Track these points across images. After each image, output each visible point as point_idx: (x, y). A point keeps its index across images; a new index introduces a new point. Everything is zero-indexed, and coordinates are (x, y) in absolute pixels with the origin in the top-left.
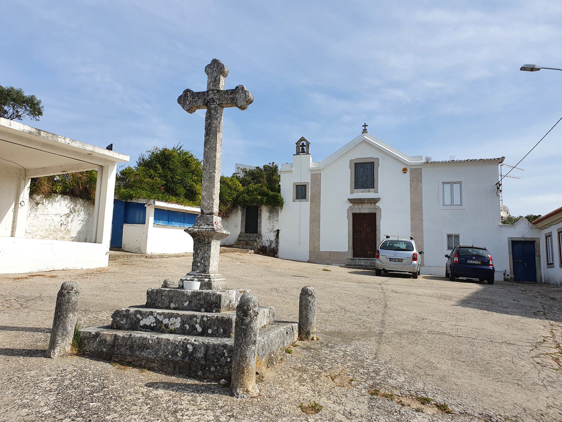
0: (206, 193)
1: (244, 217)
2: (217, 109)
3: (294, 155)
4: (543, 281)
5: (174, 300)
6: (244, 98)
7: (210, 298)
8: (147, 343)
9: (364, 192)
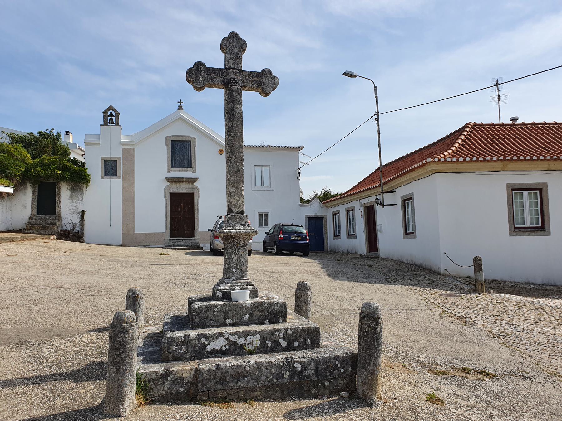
0: (233, 188)
1: (36, 196)
3: (101, 125)
4: (329, 250)
5: (230, 314)
7: (274, 307)
8: (243, 371)
9: (182, 171)
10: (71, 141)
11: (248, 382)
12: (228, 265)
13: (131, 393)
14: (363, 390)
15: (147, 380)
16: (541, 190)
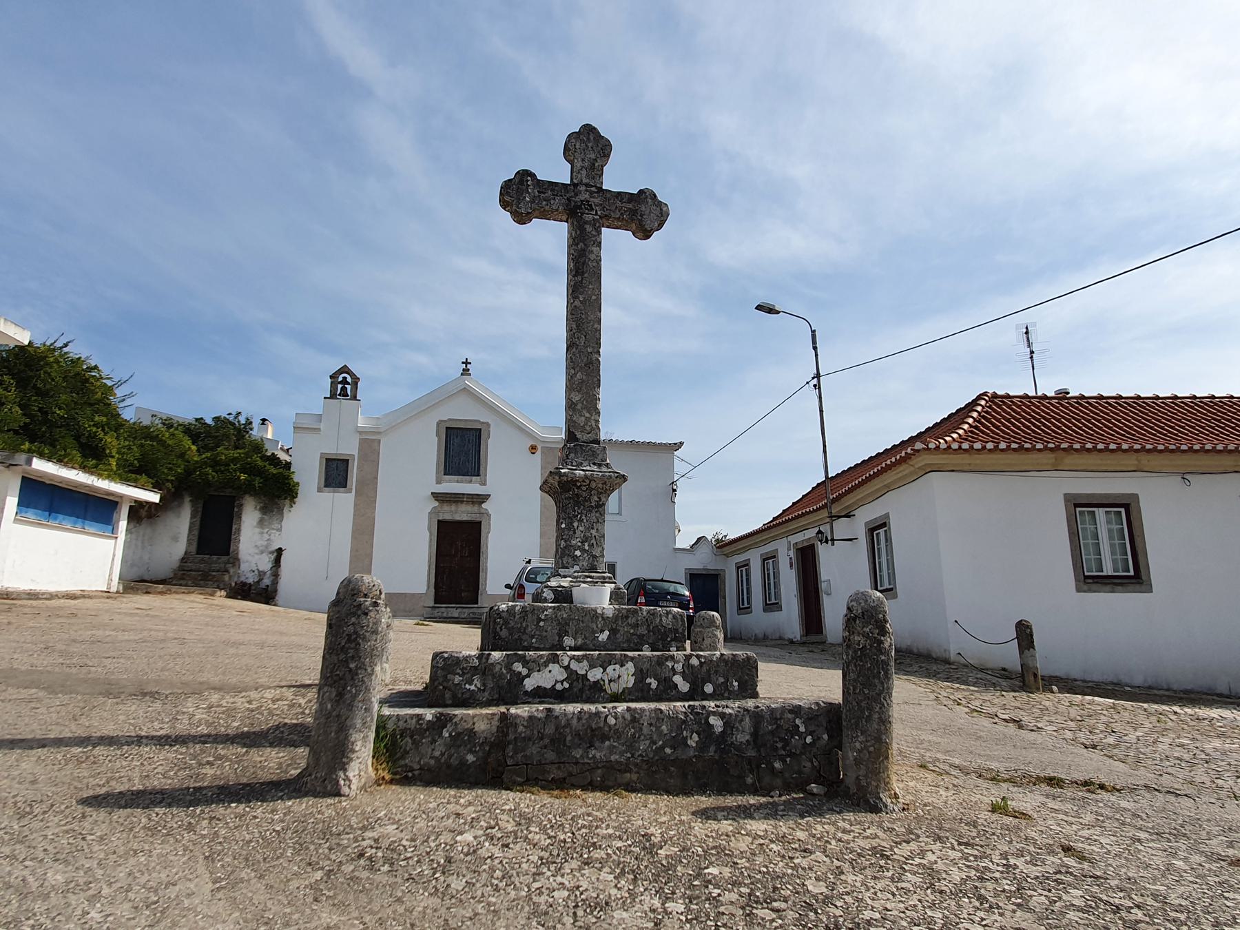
2: (597, 224)
3: (325, 398)
5: (572, 628)
6: (658, 216)
7: (661, 620)
8: (602, 724)
9: (462, 482)
10: (269, 436)
11: (612, 749)
12: (565, 542)
13: (363, 749)
14: (857, 778)
15: (398, 732)
16: (1127, 506)
